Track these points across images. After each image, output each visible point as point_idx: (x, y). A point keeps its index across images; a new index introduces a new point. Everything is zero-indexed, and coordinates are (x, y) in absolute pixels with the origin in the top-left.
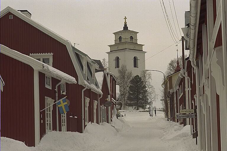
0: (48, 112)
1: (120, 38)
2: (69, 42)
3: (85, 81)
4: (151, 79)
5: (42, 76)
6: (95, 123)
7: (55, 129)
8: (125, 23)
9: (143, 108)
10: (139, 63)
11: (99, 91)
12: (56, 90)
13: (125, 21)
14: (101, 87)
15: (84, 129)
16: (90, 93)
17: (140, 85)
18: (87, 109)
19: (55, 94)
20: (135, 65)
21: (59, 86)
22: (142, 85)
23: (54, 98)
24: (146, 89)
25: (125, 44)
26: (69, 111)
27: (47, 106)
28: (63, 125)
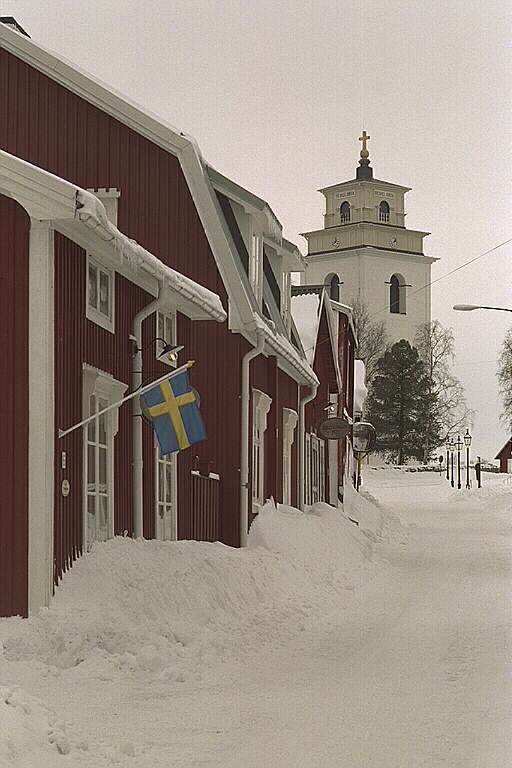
0: (97, 444)
1: (345, 207)
2: (193, 141)
3: (256, 315)
4: (454, 355)
5: (69, 256)
6: (286, 506)
7: (124, 525)
8: (364, 155)
9: (420, 459)
10: (409, 297)
11: (303, 364)
12: (137, 338)
13: (364, 147)
14: (310, 355)
15: (249, 526)
16: (270, 374)
17: (410, 373)
18: (259, 442)
19: (132, 359)
20: (396, 307)
21: (149, 325)
22: (419, 377)
23: (124, 374)
24: (435, 389)
25: (362, 227)
26: (204, 437)
27: (94, 410)
28: (161, 507)
